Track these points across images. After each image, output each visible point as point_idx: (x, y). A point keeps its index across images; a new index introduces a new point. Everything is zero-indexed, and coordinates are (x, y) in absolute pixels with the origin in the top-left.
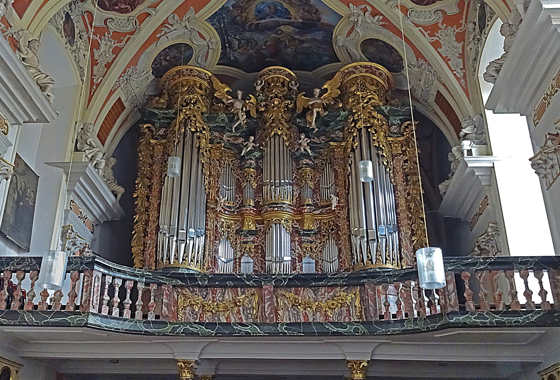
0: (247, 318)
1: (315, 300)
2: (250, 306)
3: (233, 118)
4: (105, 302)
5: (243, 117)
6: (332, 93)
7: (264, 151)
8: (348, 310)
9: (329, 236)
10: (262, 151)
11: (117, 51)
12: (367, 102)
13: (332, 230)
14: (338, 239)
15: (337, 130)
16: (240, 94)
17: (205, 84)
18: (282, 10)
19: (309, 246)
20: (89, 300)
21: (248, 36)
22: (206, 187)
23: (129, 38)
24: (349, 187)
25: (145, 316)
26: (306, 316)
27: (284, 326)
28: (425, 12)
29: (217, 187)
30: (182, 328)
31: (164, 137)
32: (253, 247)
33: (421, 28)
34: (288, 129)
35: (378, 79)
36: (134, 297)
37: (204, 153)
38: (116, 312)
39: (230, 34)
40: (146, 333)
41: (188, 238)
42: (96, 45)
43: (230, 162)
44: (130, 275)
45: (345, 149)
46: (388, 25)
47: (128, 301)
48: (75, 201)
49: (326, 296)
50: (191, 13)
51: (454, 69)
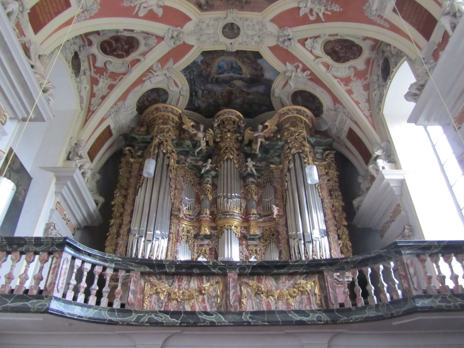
0: (211, 306)
1: (276, 288)
2: (214, 294)
3: (196, 144)
4: (71, 287)
5: (203, 144)
6: (271, 129)
7: (219, 171)
8: (309, 298)
9: (270, 240)
10: (216, 171)
11: (111, 87)
12: (298, 135)
13: (273, 235)
14: (278, 242)
15: (275, 156)
16: (202, 127)
17: (176, 119)
18: (236, 67)
19: (254, 249)
20: (54, 283)
21: (210, 87)
22: (172, 198)
23: (122, 78)
24: (286, 199)
25: (110, 304)
26: (268, 304)
27: (248, 315)
28: (342, 68)
29: (181, 198)
30: (146, 317)
31: (140, 157)
32: (208, 249)
33: (339, 80)
34: (238, 155)
35: (305, 119)
36: (102, 283)
37: (172, 170)
38: (81, 298)
39: (197, 85)
40: (111, 323)
41: (155, 239)
42: (94, 82)
43: (191, 180)
44: (100, 260)
45: (282, 170)
46: (314, 79)
47: (95, 287)
48: (61, 203)
49: (287, 284)
50: (170, 63)
51: (363, 110)
